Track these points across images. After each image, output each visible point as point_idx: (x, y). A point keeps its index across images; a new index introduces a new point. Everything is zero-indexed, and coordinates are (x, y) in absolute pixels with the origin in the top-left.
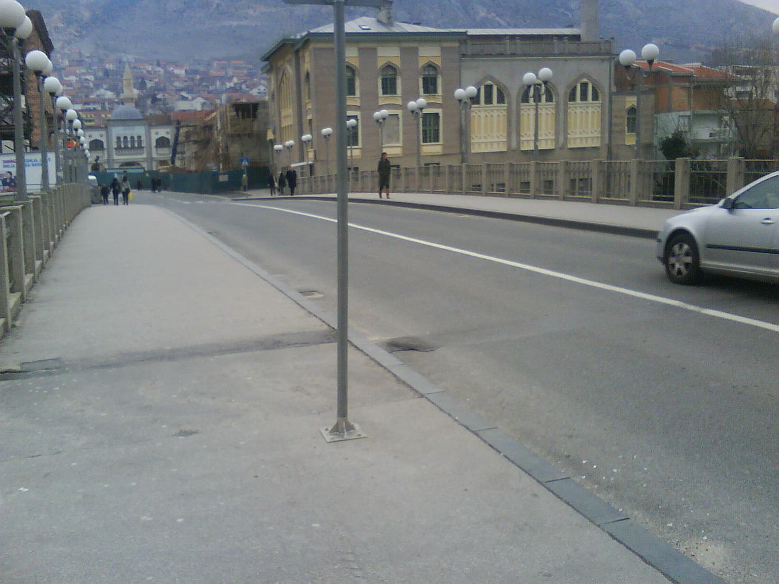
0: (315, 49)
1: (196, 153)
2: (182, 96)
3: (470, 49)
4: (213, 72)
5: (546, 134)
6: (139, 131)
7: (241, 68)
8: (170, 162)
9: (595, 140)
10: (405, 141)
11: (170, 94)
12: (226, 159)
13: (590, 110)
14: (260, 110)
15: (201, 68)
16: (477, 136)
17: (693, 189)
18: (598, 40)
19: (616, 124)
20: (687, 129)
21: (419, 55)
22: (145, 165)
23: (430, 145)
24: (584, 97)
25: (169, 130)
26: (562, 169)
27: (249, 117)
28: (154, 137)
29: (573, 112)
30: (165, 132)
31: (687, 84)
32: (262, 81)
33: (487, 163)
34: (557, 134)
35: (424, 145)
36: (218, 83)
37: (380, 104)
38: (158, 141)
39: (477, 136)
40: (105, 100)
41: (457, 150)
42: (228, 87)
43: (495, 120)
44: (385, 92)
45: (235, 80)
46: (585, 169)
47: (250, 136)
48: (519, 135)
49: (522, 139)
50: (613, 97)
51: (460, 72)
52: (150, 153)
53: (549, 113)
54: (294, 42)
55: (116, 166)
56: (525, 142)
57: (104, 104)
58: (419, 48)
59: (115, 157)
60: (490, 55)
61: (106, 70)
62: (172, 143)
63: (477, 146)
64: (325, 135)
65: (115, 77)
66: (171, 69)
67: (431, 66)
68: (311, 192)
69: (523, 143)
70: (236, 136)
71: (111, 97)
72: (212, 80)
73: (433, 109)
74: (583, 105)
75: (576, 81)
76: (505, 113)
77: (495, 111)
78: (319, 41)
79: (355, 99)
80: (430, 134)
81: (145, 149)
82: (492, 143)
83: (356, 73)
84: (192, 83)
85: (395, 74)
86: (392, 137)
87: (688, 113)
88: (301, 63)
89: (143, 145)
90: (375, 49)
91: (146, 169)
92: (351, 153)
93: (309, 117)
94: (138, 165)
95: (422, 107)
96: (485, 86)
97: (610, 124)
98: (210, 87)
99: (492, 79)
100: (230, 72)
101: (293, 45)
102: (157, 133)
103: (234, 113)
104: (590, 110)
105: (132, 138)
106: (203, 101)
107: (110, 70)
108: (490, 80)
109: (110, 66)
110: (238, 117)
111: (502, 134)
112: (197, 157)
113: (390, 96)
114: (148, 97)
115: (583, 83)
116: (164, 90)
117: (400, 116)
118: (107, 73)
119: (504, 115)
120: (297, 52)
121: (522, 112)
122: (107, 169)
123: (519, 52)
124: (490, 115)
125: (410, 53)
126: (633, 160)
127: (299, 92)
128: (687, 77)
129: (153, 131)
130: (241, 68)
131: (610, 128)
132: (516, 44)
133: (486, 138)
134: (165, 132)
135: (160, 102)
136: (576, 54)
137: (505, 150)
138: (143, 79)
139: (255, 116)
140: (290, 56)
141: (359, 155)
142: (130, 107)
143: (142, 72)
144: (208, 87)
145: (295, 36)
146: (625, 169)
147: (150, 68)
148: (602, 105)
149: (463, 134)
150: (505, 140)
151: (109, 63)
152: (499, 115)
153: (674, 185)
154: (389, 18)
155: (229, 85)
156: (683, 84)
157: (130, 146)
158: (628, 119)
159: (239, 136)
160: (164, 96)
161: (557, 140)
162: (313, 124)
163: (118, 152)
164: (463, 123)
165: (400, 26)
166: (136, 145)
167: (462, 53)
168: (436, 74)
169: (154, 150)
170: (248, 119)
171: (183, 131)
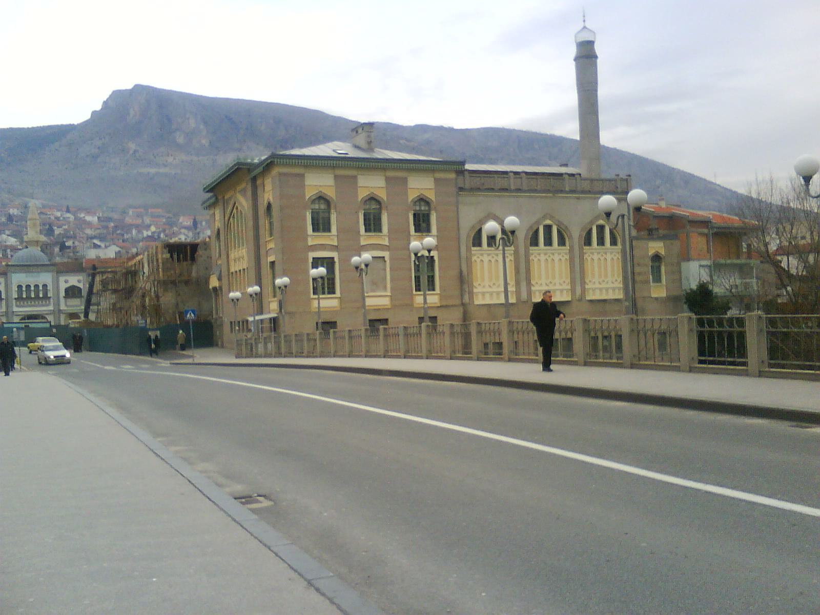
0: (280, 174)
1: (114, 304)
2: (94, 243)
3: (468, 182)
4: (128, 220)
5: (546, 284)
6: (45, 278)
7: (158, 216)
8: (82, 316)
10: (392, 289)
11: (80, 242)
12: (157, 310)
14: (200, 252)
15: (116, 216)
17: (773, 352)
18: (613, 177)
19: (639, 274)
20: (709, 279)
22: (50, 318)
25: (81, 278)
26: (579, 327)
27: (185, 259)
28: (63, 286)
30: (75, 280)
31: (706, 231)
32: (183, 230)
33: (583, 317)
34: (573, 282)
36: (134, 232)
37: (362, 243)
38: (67, 290)
40: (7, 247)
41: (458, 302)
42: (145, 235)
43: (543, 264)
44: (367, 230)
45: (153, 229)
46: (568, 327)
47: (187, 283)
49: (533, 288)
50: (634, 243)
51: (458, 208)
52: (57, 304)
53: (563, 259)
54: (250, 168)
55: (16, 319)
57: (5, 251)
59: (15, 309)
60: (492, 190)
61: (10, 215)
62: (84, 293)
63: (480, 296)
64: (279, 286)
65: (19, 223)
66: (82, 215)
68: (279, 355)
69: (535, 293)
70: (168, 284)
71: (14, 244)
72: (128, 228)
75: (592, 223)
78: (287, 165)
79: (331, 237)
81: (51, 299)
82: (607, 289)
83: (332, 206)
84: (105, 231)
85: (380, 209)
86: (378, 284)
89: (49, 296)
90: (355, 178)
91: (53, 324)
92: (319, 303)
93: (271, 259)
94: (42, 319)
95: (429, 248)
96: (597, 226)
97: (633, 273)
98: (125, 235)
100: (147, 221)
102: (66, 282)
103: (168, 255)
104: (609, 257)
105: (37, 286)
106: (118, 249)
107: (14, 215)
109: (14, 211)
110: (173, 260)
112: (114, 308)
113: (374, 234)
114: (55, 244)
116: (74, 237)
117: (387, 259)
118: (10, 218)
119: (566, 259)
120: (254, 179)
121: (586, 256)
122: (5, 323)
123: (525, 187)
124: (479, 260)
126: (503, 320)
127: (256, 228)
128: (705, 223)
129: (62, 279)
130: (158, 216)
131: (630, 279)
132: (521, 178)
133: (548, 286)
134: (75, 280)
135: (68, 250)
136: (589, 192)
138: (50, 225)
139: (193, 259)
140: (246, 185)
142: (36, 251)
143: (50, 218)
144: (123, 235)
146: (615, 327)
147: (59, 214)
148: (571, 250)
149: (463, 281)
150: (569, 287)
151: (13, 208)
152: (490, 261)
154: (370, 143)
155: (146, 233)
157: (33, 296)
159: (174, 283)
160: (73, 243)
161: (573, 291)
162: (277, 265)
163: (18, 303)
165: (383, 153)
166: (41, 295)
167: (462, 186)
168: (430, 210)
169: (62, 301)
170: (185, 263)
171: (98, 278)
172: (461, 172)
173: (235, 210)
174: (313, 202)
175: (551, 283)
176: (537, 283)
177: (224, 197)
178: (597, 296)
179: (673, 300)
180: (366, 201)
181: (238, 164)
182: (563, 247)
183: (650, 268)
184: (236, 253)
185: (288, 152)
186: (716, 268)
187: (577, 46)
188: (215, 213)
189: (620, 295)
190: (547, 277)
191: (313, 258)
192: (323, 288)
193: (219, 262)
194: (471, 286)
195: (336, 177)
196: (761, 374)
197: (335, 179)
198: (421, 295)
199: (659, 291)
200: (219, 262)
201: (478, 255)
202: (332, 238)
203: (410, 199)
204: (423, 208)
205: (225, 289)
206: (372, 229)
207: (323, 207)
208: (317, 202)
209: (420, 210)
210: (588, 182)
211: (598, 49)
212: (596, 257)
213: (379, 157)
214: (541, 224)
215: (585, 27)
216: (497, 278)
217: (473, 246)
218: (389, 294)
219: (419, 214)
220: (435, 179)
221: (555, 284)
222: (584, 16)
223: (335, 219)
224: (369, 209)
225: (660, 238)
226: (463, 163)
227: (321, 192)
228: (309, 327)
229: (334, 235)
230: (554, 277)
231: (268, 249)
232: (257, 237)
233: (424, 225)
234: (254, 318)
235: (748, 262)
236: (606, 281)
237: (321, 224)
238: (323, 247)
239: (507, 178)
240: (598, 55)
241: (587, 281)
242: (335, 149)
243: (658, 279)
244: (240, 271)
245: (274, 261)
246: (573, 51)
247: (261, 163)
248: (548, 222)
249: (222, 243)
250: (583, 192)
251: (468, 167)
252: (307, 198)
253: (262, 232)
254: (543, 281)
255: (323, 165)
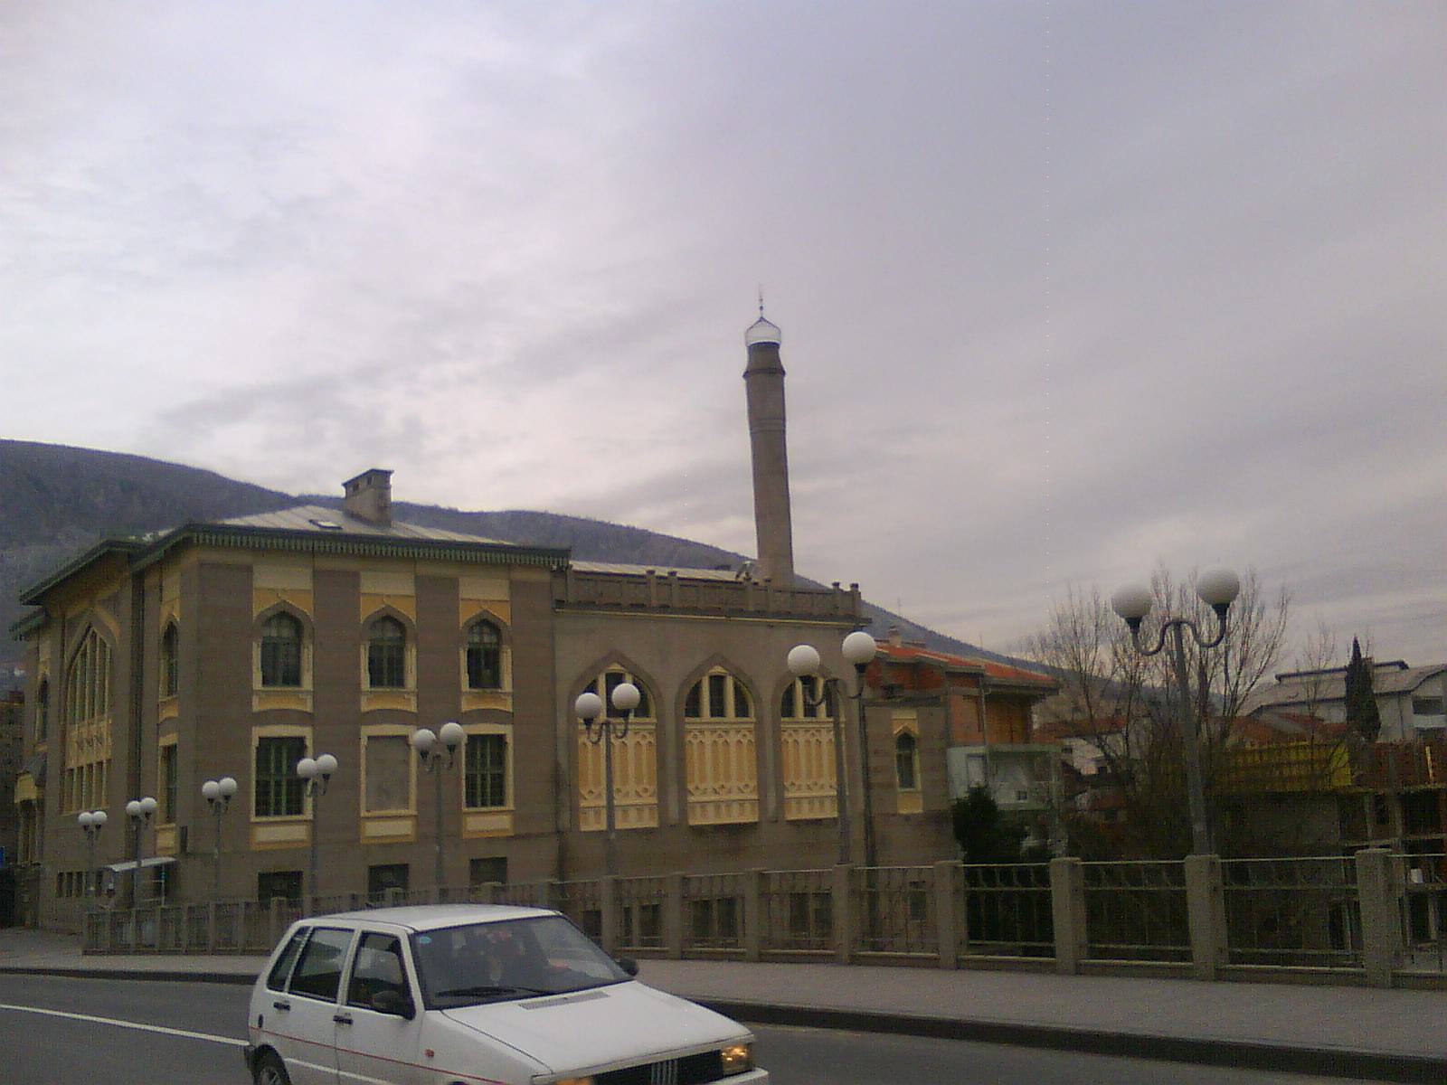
0: (202, 565)
5: (739, 789)
9: (747, 805)
10: (420, 803)
13: (733, 738)
16: (591, 792)
21: (362, 591)
23: (484, 812)
24: (718, 710)
29: (695, 742)
31: (974, 691)
34: (761, 788)
35: (469, 813)
39: (591, 792)
43: (733, 749)
48: (683, 791)
50: (869, 711)
53: (745, 741)
54: (134, 553)
56: (793, 804)
58: (362, 573)
60: (618, 606)
63: (698, 809)
67: (486, 623)
73: (294, 727)
74: (811, 726)
76: (751, 737)
77: (801, 732)
80: (483, 786)
82: (729, 804)
83: (307, 632)
85: (403, 639)
87: (981, 750)
88: (150, 601)
90: (355, 576)
93: (167, 740)
96: (607, 675)
97: (866, 768)
99: (622, 660)
101: (131, 558)
104: (733, 738)
108: (720, 665)
111: (648, 787)
113: (279, 689)
115: (715, 676)
119: (750, 741)
120: (139, 577)
121: (785, 736)
123: (676, 603)
125: (437, 592)
127: (138, 676)
133: (743, 792)
136: (788, 615)
137: (654, 824)
141: (305, 838)
145: (139, 537)
148: (759, 724)
149: (561, 784)
150: (654, 800)
152: (715, 742)
153: (415, 966)
156: (965, 690)
158: (899, 756)
161: (762, 802)
162: (182, 761)
164: (563, 760)
167: (558, 597)
168: (499, 643)
172: (563, 571)
173: (88, 641)
174: (268, 622)
175: (723, 787)
176: (697, 788)
177: (64, 616)
178: (806, 814)
179: (934, 818)
180: (269, 620)
181: (110, 544)
182: (745, 719)
183: (895, 759)
184: (84, 730)
185: (229, 522)
186: (993, 761)
187: (749, 353)
188: (38, 648)
189: (830, 812)
190: (716, 779)
191: (261, 739)
192: (483, 794)
193: (42, 749)
194: (575, 795)
195: (317, 574)
196: (1079, 971)
197: (510, 588)
198: (172, 829)
199: (910, 805)
200: (42, 749)
201: (645, 733)
202: (302, 698)
203: (463, 619)
204: (486, 639)
205: (52, 803)
206: (385, 681)
207: (286, 633)
208: (274, 622)
209: (481, 642)
210: (789, 595)
211: (786, 357)
212: (802, 738)
213: (402, 535)
214: (704, 675)
215: (762, 319)
216: (597, 783)
217: (687, 716)
218: (412, 811)
219: (478, 652)
220: (417, 577)
221: (627, 794)
222: (761, 300)
223: (311, 660)
224: (382, 640)
225: (909, 703)
226: (565, 554)
227: (388, 606)
228: (244, 887)
229: (307, 692)
230: (728, 777)
231: (161, 720)
232: (137, 693)
233: (487, 673)
234: (139, 864)
235: (1046, 750)
236: (624, 792)
237: (283, 673)
238: (282, 716)
239: (645, 583)
240: (786, 370)
241: (690, 787)
242: (312, 518)
243: (908, 781)
244: (90, 766)
245: (175, 746)
246: (742, 361)
247: (158, 544)
248: (718, 670)
249: (53, 712)
250: (778, 614)
251: (578, 565)
252: (255, 615)
253: (148, 684)
254: (709, 784)
255: (532, 563)
